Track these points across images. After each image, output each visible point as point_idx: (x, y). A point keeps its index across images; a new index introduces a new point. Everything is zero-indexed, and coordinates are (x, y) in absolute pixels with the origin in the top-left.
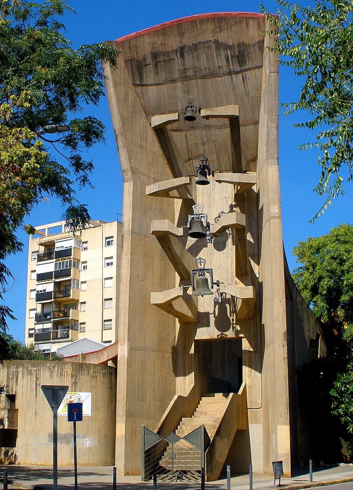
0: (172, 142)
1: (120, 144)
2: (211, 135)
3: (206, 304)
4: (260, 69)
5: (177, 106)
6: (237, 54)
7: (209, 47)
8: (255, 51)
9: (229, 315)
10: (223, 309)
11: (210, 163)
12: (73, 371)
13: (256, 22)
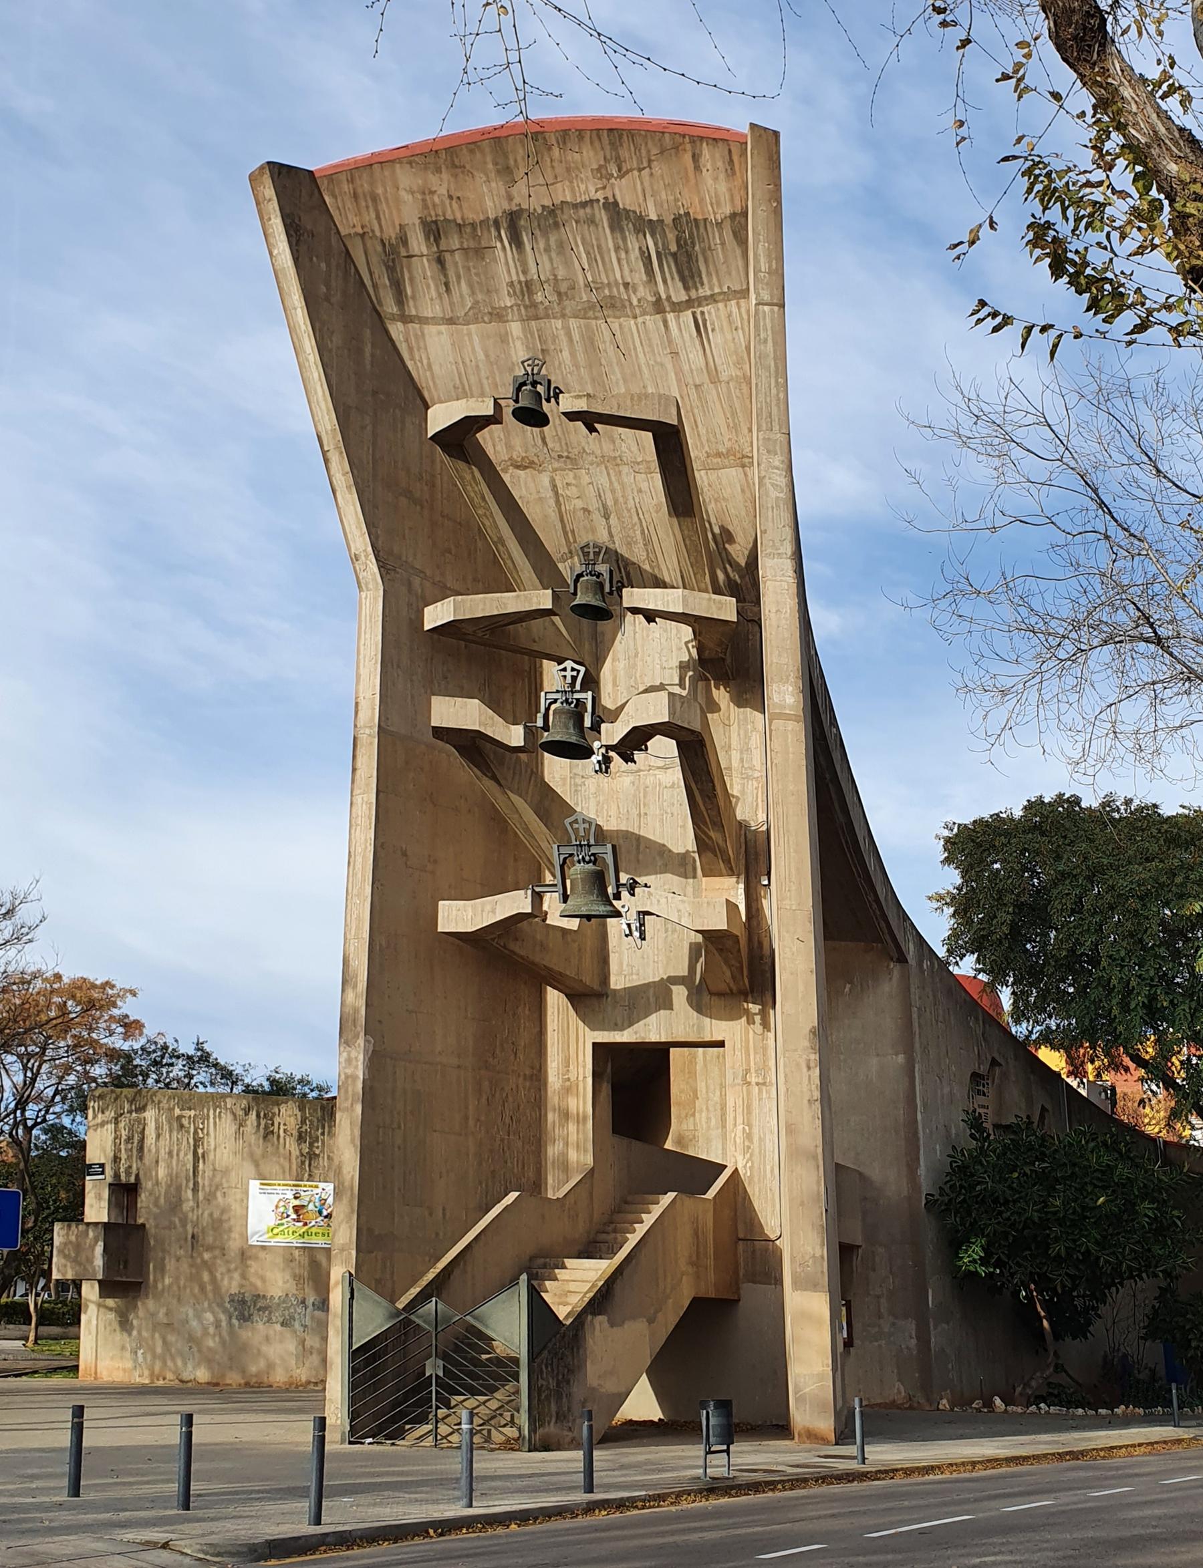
7: (592, 221)
8: (723, 244)
12: (303, 1122)
13: (721, 150)
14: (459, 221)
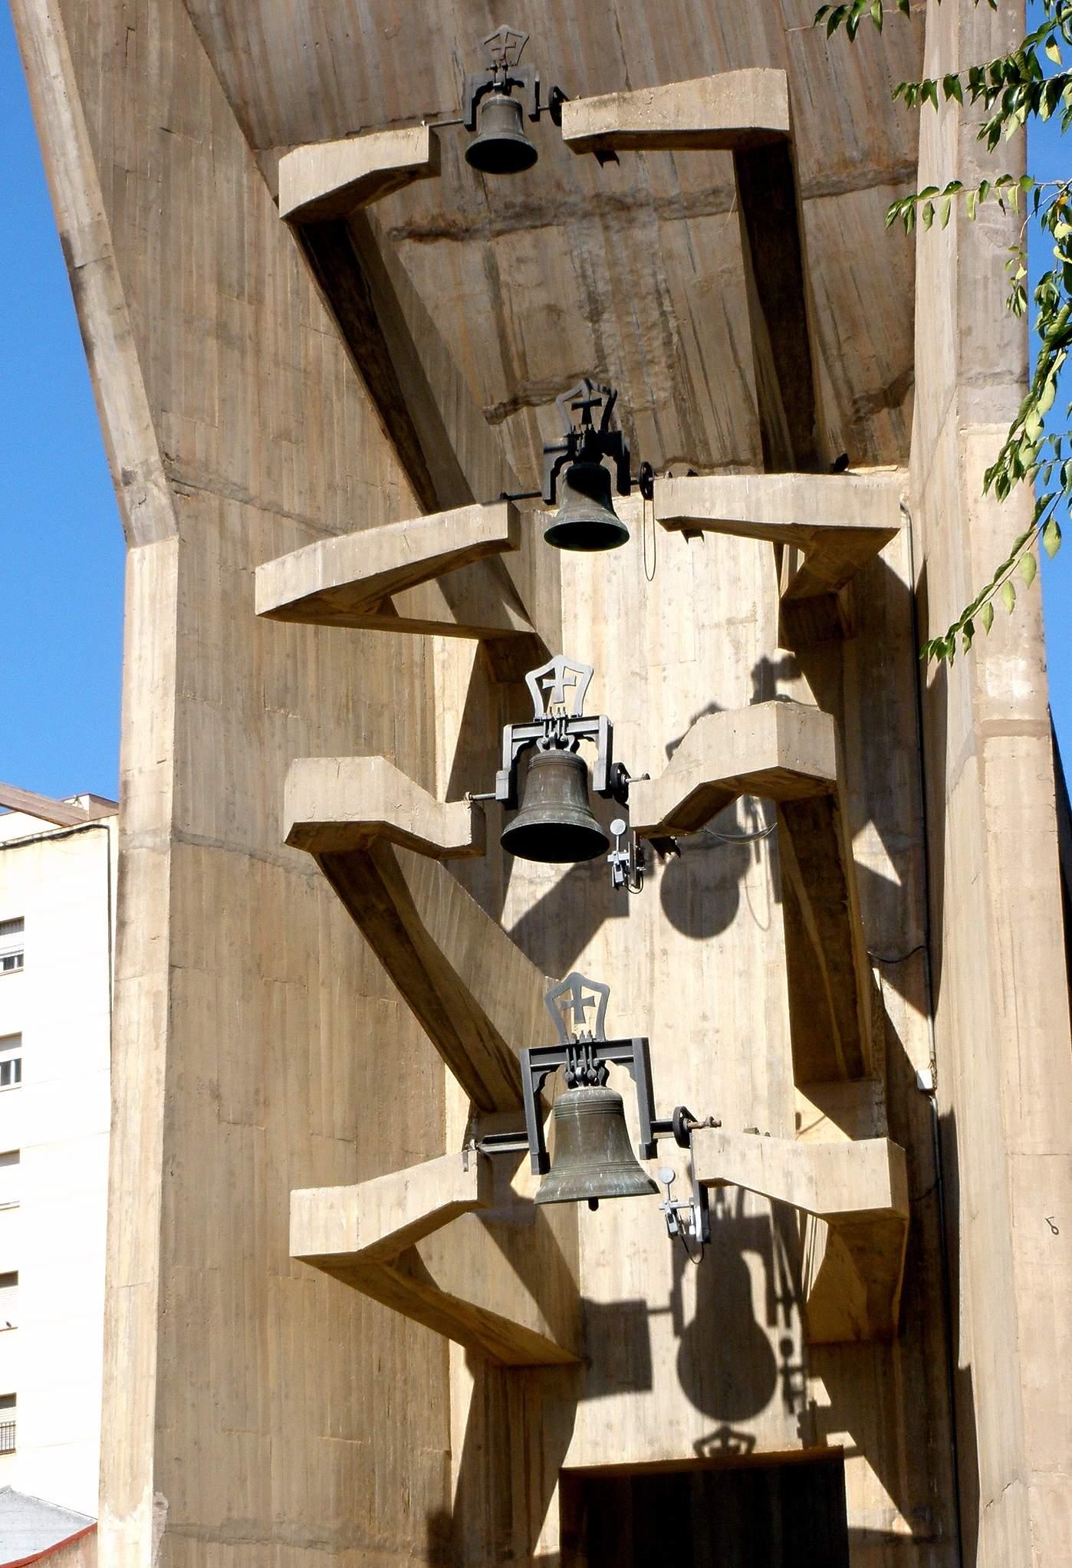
0: (398, 288)
1: (101, 322)
2: (635, 258)
3: (624, 1254)
5: (433, 91)
10: (724, 1289)
11: (637, 421)
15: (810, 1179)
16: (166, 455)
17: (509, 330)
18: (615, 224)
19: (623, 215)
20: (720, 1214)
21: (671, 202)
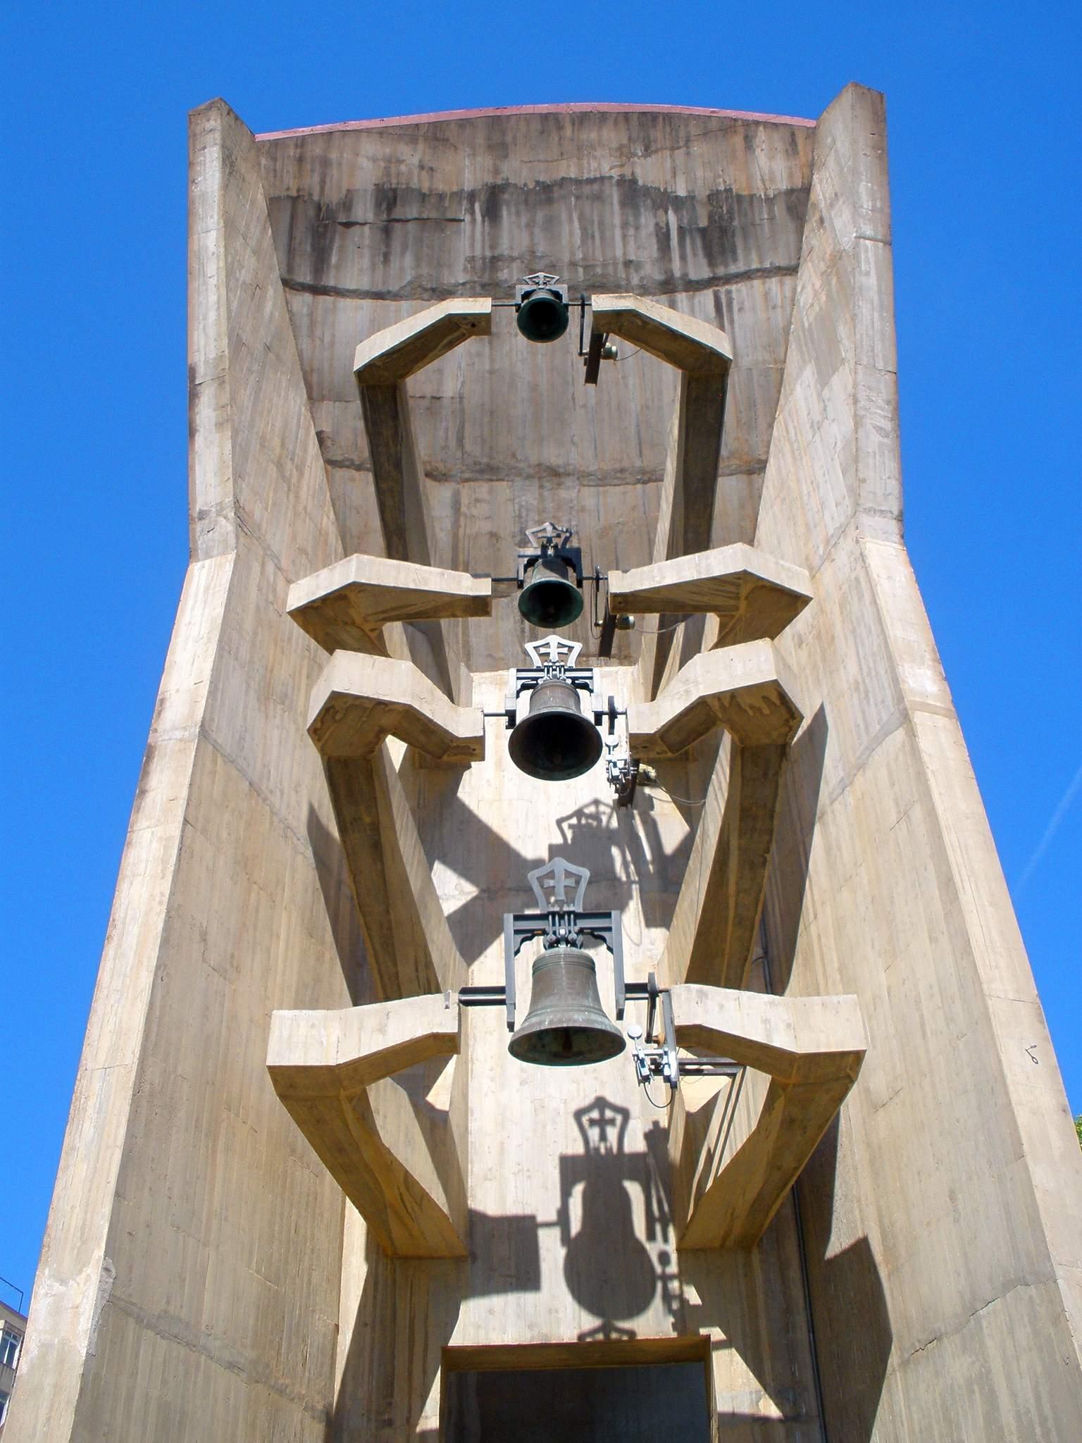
2: (559, 508)
4: (788, 280)
5: (440, 383)
6: (703, 223)
9: (640, 1229)
10: (606, 1212)
14: (425, 190)
15: (789, 1025)
16: (237, 502)
17: (460, 545)
18: (547, 485)
19: (556, 480)
20: (603, 1151)
21: (590, 475)
